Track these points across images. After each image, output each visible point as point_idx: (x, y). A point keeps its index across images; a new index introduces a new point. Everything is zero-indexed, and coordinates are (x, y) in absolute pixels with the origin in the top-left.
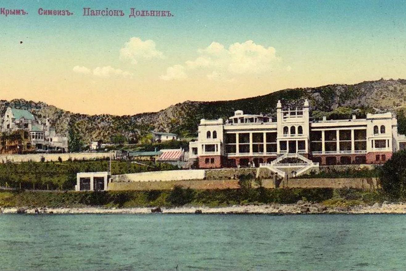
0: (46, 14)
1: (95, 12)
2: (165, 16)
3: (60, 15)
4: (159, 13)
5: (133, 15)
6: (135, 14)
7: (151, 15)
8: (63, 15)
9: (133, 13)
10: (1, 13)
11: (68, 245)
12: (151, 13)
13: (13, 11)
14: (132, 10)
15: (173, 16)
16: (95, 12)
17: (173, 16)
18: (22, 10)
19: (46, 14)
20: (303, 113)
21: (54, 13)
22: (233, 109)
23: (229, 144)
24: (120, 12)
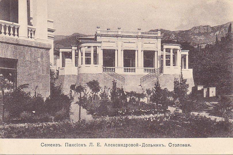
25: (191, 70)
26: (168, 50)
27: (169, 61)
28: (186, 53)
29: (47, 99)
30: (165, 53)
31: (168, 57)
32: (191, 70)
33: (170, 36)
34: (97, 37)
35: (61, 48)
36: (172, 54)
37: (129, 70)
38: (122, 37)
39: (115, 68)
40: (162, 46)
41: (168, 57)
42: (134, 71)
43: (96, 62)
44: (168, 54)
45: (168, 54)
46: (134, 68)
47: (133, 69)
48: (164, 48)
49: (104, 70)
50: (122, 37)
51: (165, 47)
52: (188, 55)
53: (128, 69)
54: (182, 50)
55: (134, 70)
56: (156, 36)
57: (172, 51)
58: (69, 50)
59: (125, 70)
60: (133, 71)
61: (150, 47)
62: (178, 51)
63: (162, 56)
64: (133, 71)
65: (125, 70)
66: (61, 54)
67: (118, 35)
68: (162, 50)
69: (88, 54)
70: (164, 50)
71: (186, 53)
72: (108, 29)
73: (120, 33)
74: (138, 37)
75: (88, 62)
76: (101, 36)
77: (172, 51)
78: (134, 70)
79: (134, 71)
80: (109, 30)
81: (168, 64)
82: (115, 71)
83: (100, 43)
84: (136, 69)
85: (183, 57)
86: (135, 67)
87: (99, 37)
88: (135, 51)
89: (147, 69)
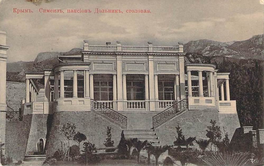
12: (109, 11)
26: (195, 73)
27: (197, 89)
28: (226, 76)
29: (209, 138)
31: (195, 83)
34: (84, 56)
36: (201, 78)
41: (195, 83)
42: (143, 106)
43: (81, 95)
46: (144, 101)
47: (104, 103)
51: (190, 68)
52: (229, 80)
53: (139, 103)
55: (143, 105)
56: (176, 52)
57: (200, 74)
59: (130, 106)
60: (136, 106)
61: (169, 70)
63: (186, 82)
65: (130, 106)
68: (186, 73)
69: (69, 83)
70: (189, 73)
71: (226, 76)
73: (151, 50)
74: (116, 54)
75: (69, 94)
77: (200, 74)
79: (143, 106)
80: (109, 45)
81: (196, 93)
83: (88, 64)
84: (114, 103)
85: (221, 82)
88: (144, 76)
89: (142, 102)
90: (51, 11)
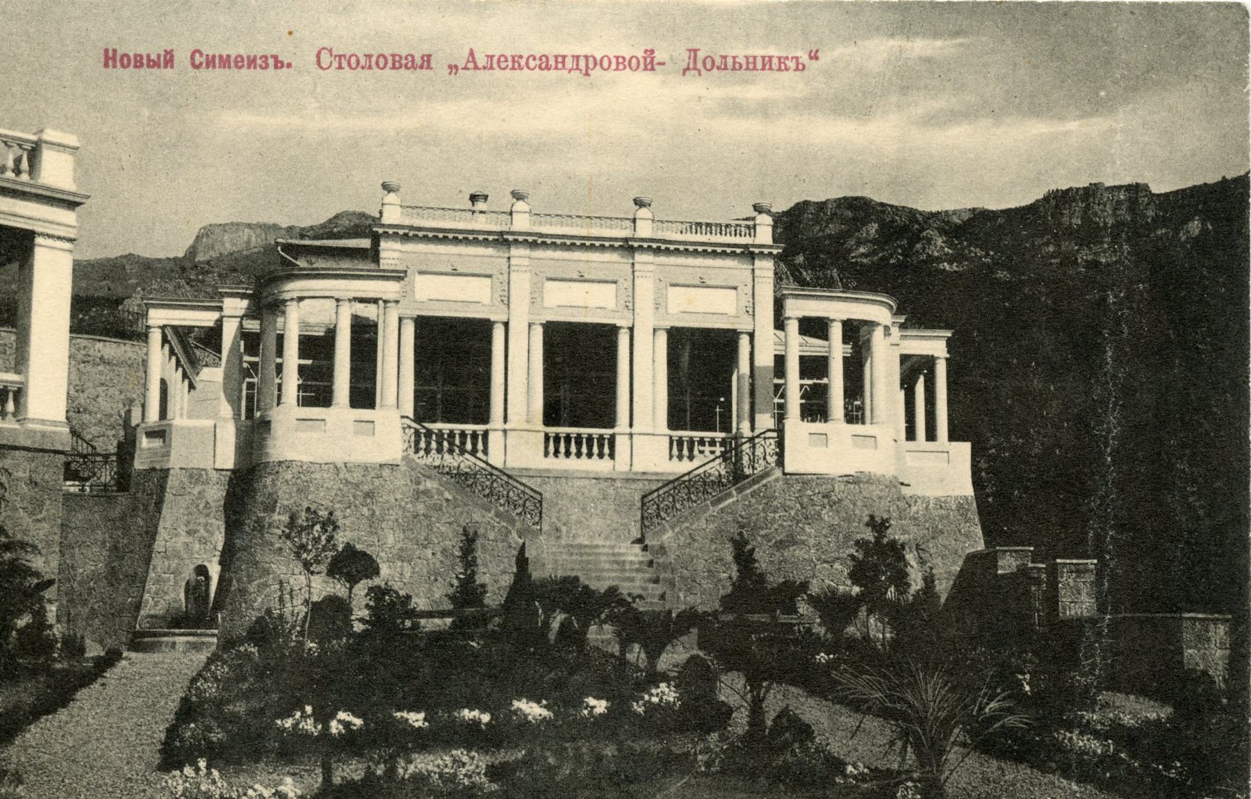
0: (229, 67)
1: (552, 62)
2: (787, 69)
3: (255, 68)
4: (764, 65)
5: (695, 68)
6: (700, 65)
7: (747, 69)
8: (261, 67)
9: (695, 62)
10: (106, 65)
11: (281, 599)
13: (153, 57)
14: (692, 55)
15: (289, 65)
16: (552, 62)
17: (289, 65)
18: (275, 57)
19: (229, 67)
20: (818, 426)
21: (243, 61)
22: (1001, 274)
23: (212, 595)
24: (794, 60)
25: (965, 448)
26: (814, 327)
28: (934, 345)
30: (797, 346)
31: (814, 367)
32: (965, 448)
33: (916, 238)
34: (383, 244)
35: (154, 306)
36: (837, 350)
37: (590, 448)
38: (535, 242)
39: (486, 435)
40: (779, 305)
41: (814, 367)
42: (606, 450)
43: (363, 396)
44: (815, 346)
45: (815, 346)
47: (451, 434)
48: (150, 322)
49: (421, 441)
50: (535, 242)
51: (797, 308)
52: (947, 359)
54: (903, 326)
57: (836, 332)
58: (206, 319)
59: (554, 445)
60: (428, 444)
62: (878, 335)
63: (780, 361)
64: (428, 444)
65: (554, 445)
66: (156, 336)
67: (508, 233)
68: (780, 324)
70: (793, 327)
71: (934, 345)
72: (474, 198)
76: (408, 235)
77: (836, 332)
78: (608, 447)
79: (606, 450)
80: (481, 205)
81: (815, 408)
82: (485, 452)
83: (398, 276)
86: (616, 430)
87: (397, 245)
88: (613, 330)
89: (681, 438)
90: (122, 59)
